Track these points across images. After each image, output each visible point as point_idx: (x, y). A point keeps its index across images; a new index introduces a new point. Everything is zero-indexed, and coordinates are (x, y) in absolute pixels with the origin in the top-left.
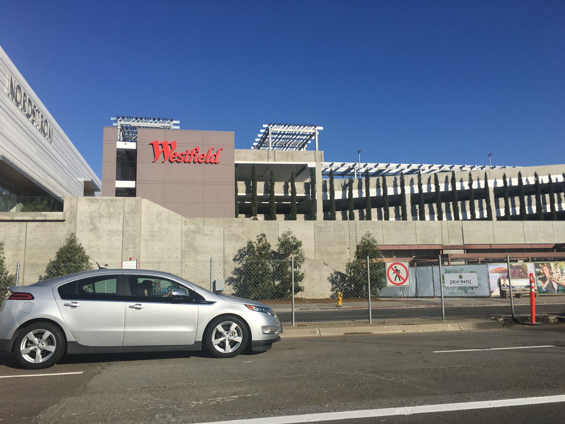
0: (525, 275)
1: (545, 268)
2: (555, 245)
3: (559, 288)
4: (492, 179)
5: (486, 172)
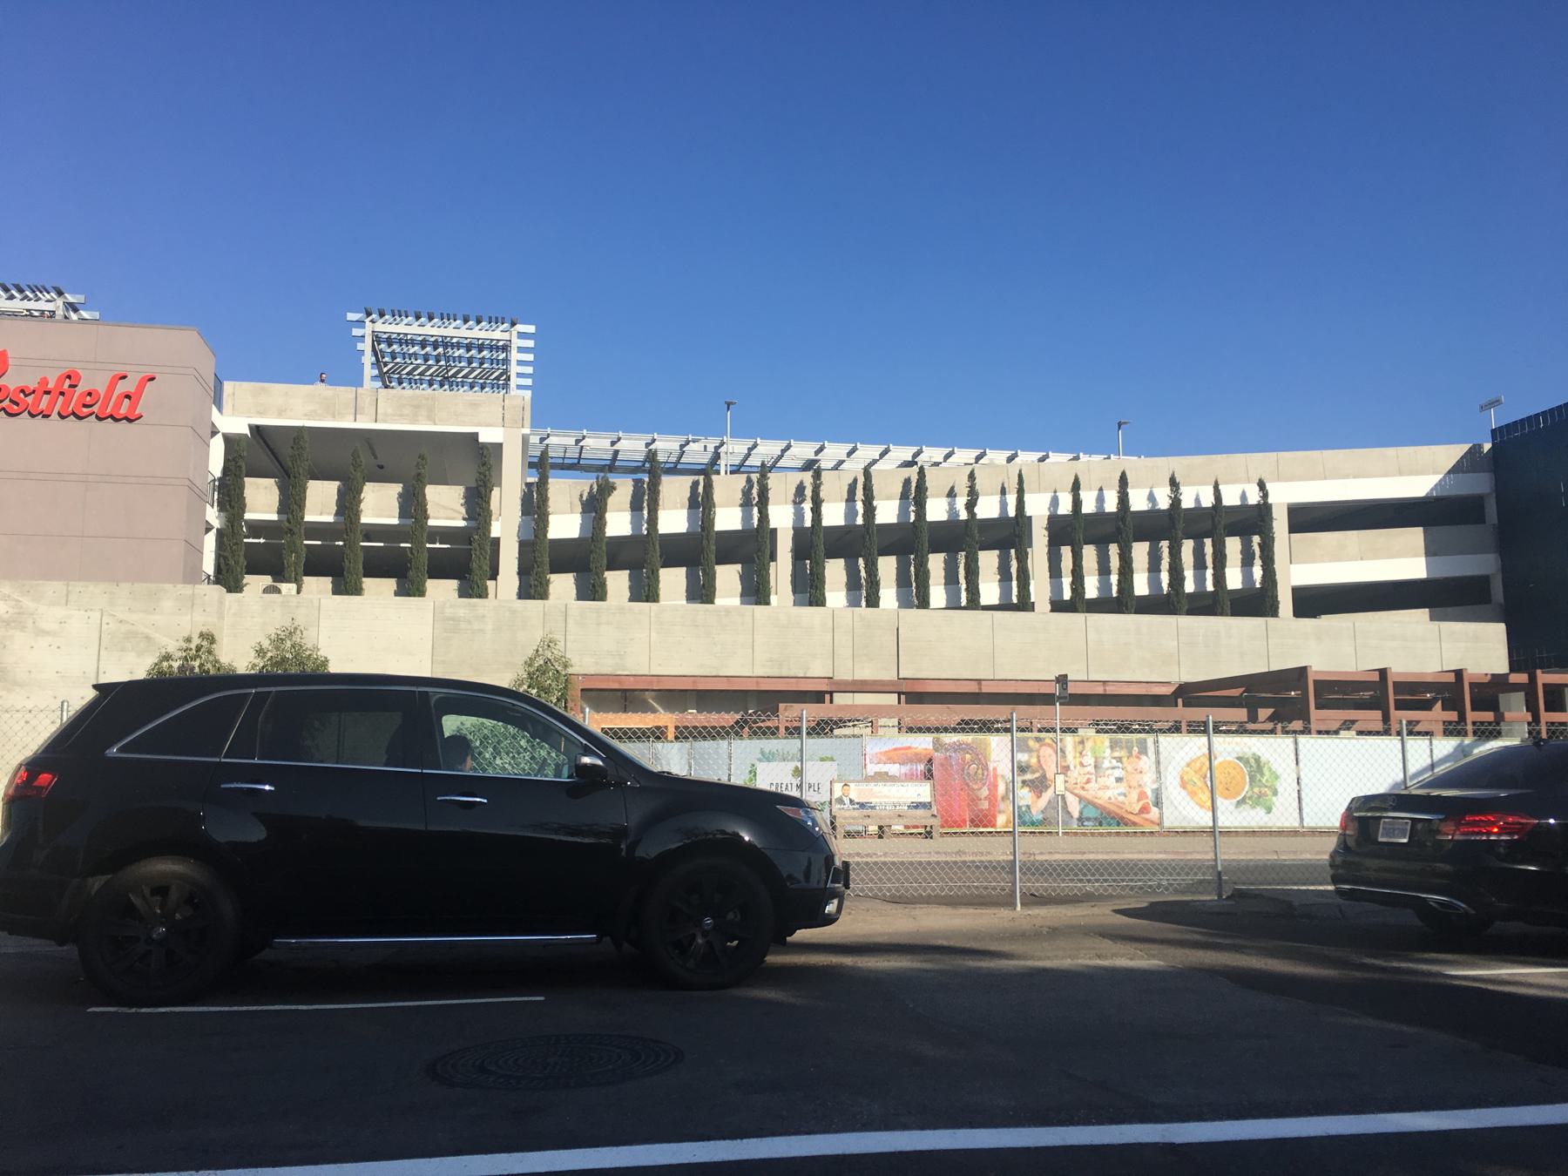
0: (980, 771)
1: (1047, 752)
3: (1085, 815)
4: (1046, 491)
5: (1020, 471)
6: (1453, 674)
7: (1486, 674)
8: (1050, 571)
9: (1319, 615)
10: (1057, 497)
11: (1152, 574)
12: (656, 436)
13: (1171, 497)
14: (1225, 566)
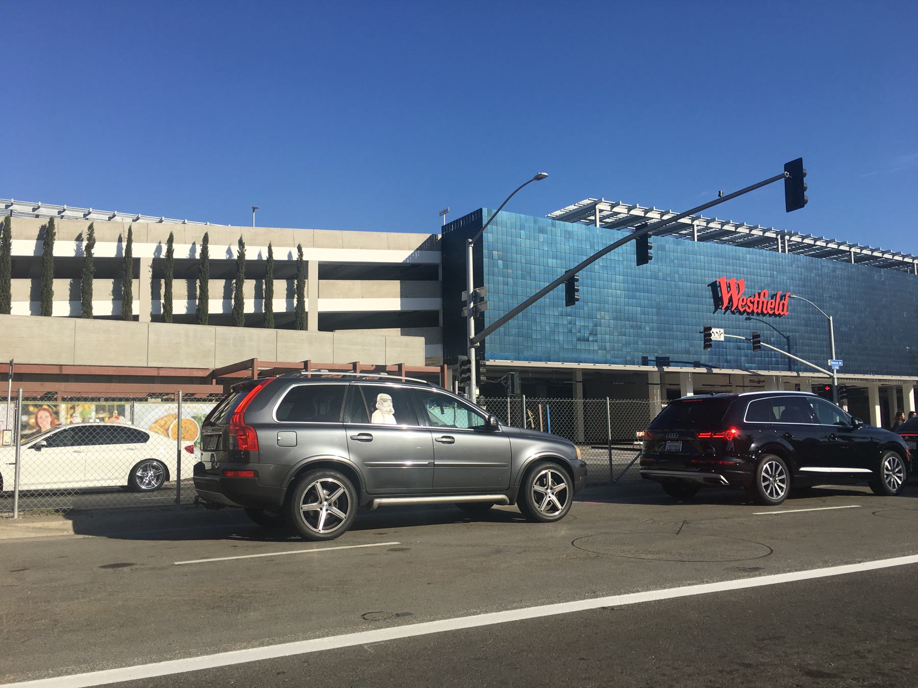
2: (214, 371)
4: (152, 241)
5: (130, 227)
6: (397, 366)
7: (373, 365)
8: (152, 295)
9: (335, 330)
10: (161, 246)
11: (190, 300)
12: (91, 210)
13: (239, 252)
14: (272, 297)
